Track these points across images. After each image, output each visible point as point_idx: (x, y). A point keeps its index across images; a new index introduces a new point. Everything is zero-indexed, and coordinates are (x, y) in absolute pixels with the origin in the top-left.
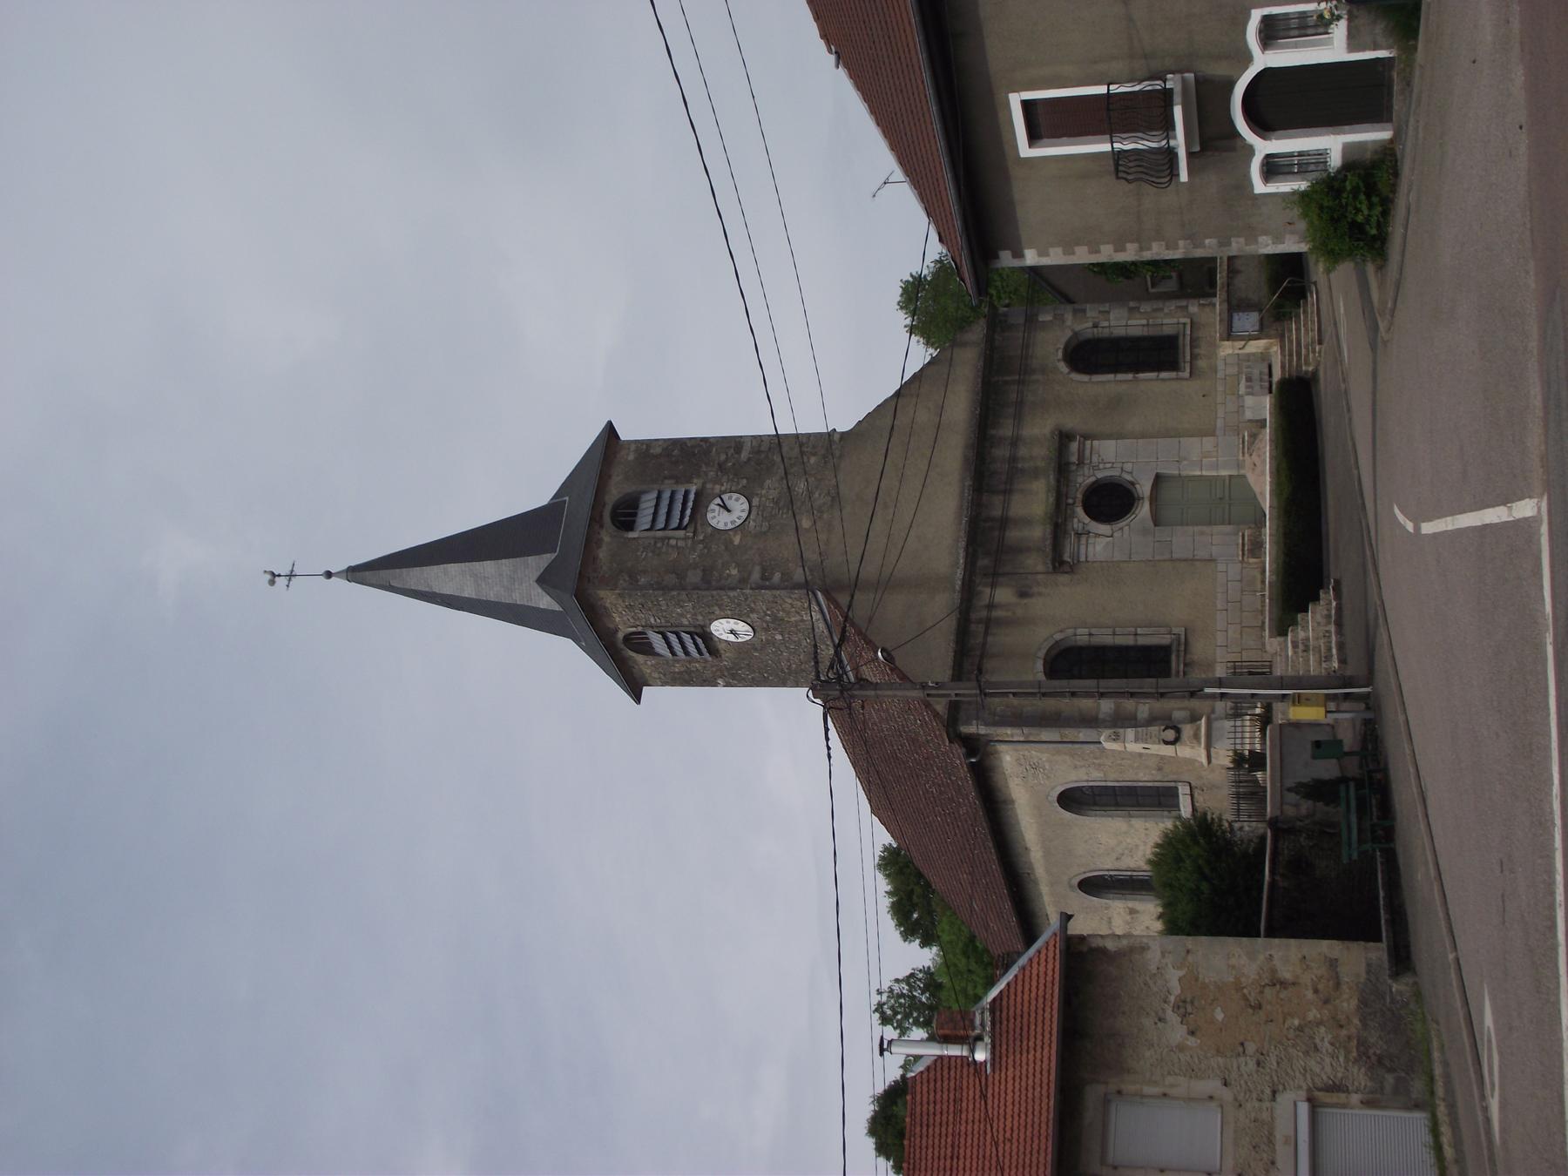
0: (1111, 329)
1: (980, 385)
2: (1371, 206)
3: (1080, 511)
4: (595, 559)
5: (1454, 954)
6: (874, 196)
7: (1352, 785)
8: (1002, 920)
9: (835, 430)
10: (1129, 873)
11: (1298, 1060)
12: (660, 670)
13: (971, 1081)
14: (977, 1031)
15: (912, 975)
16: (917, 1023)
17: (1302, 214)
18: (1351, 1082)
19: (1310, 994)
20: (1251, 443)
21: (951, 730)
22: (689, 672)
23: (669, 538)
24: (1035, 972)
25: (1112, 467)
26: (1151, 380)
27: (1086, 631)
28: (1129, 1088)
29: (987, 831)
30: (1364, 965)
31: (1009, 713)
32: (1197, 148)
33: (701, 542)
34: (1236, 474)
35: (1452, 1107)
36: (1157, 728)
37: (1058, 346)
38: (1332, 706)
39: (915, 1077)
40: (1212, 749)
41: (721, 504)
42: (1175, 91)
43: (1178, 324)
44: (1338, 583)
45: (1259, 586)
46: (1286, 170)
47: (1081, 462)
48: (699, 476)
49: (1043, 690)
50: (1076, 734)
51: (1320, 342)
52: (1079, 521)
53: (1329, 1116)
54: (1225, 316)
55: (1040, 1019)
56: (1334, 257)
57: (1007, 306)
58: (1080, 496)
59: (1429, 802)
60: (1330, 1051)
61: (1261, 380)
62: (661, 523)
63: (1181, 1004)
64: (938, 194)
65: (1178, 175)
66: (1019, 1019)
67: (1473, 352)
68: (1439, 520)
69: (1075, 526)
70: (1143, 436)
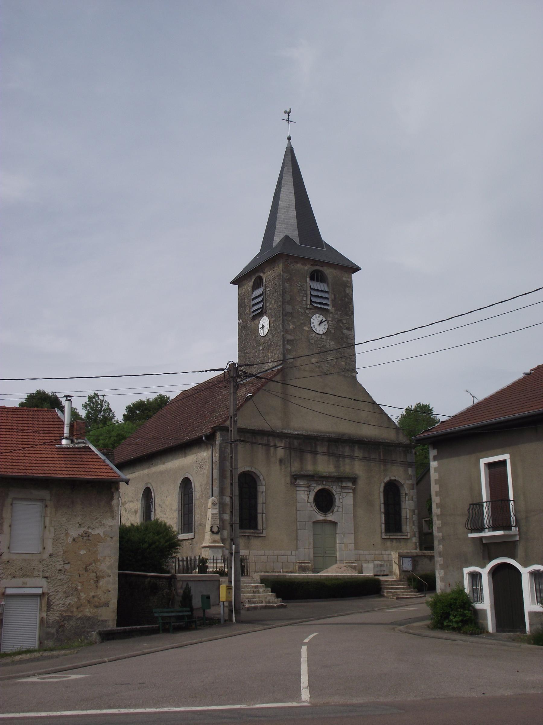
0: (404, 502)
1: (378, 441)
2: (457, 622)
3: (320, 487)
4: (297, 262)
5: (107, 661)
6: (467, 391)
7: (190, 613)
8: (132, 452)
9: (357, 373)
10: (153, 510)
11: (62, 588)
12: (246, 293)
13: (53, 438)
14: (75, 441)
15: (111, 411)
16: (89, 413)
17: (454, 590)
18: (52, 613)
19: (92, 594)
20: (351, 567)
21: (218, 428)
22: (245, 306)
23: (306, 297)
24: (102, 467)
25: (340, 502)
26: (381, 520)
27: (264, 490)
28: (48, 510)
29: (172, 445)
30: (106, 619)
31: (226, 455)
32: (484, 542)
33: (305, 312)
34: (337, 560)
35: (38, 659)
36: (218, 523)
37: (397, 477)
38: (226, 604)
39: (56, 412)
40: (208, 549)
41: (323, 321)
42: (511, 531)
43: (407, 533)
44: (285, 607)
45: (285, 570)
46: (474, 583)
47: (342, 488)
48: (336, 310)
49: (233, 470)
50: (216, 486)
51: (397, 599)
52: (315, 487)
53: (35, 604)
54: (410, 555)
55: (80, 470)
56: (433, 605)
57: (415, 453)
58: (327, 487)
59: (179, 649)
60: (66, 603)
61: (381, 571)
62: (313, 293)
63: (87, 535)
64: (463, 421)
65: (471, 533)
66: (80, 460)
67: (382, 671)
68: (307, 655)
69: (313, 485)
70: (355, 516)
